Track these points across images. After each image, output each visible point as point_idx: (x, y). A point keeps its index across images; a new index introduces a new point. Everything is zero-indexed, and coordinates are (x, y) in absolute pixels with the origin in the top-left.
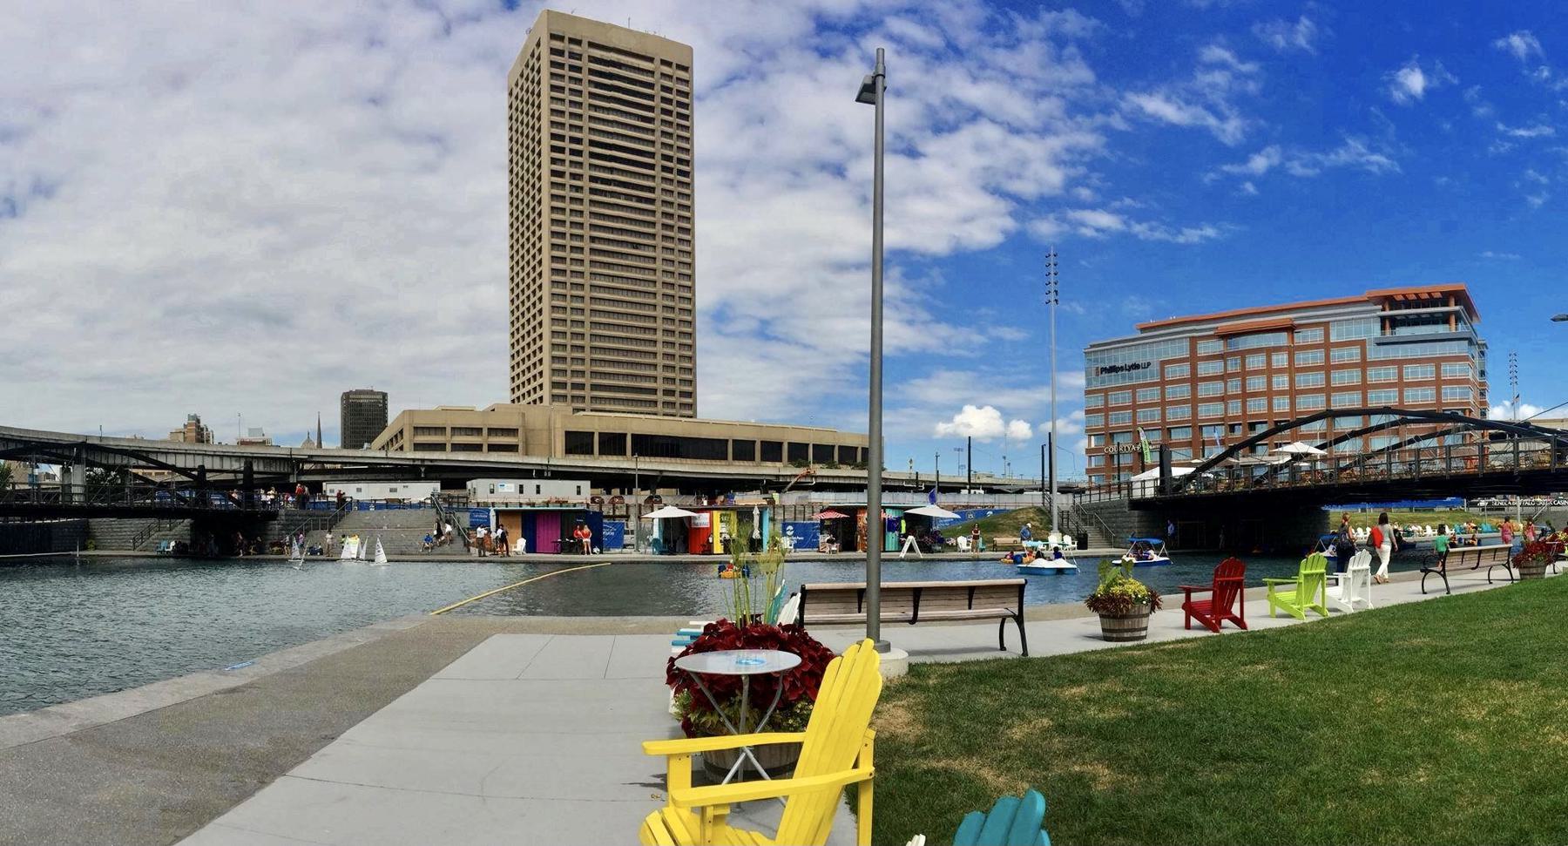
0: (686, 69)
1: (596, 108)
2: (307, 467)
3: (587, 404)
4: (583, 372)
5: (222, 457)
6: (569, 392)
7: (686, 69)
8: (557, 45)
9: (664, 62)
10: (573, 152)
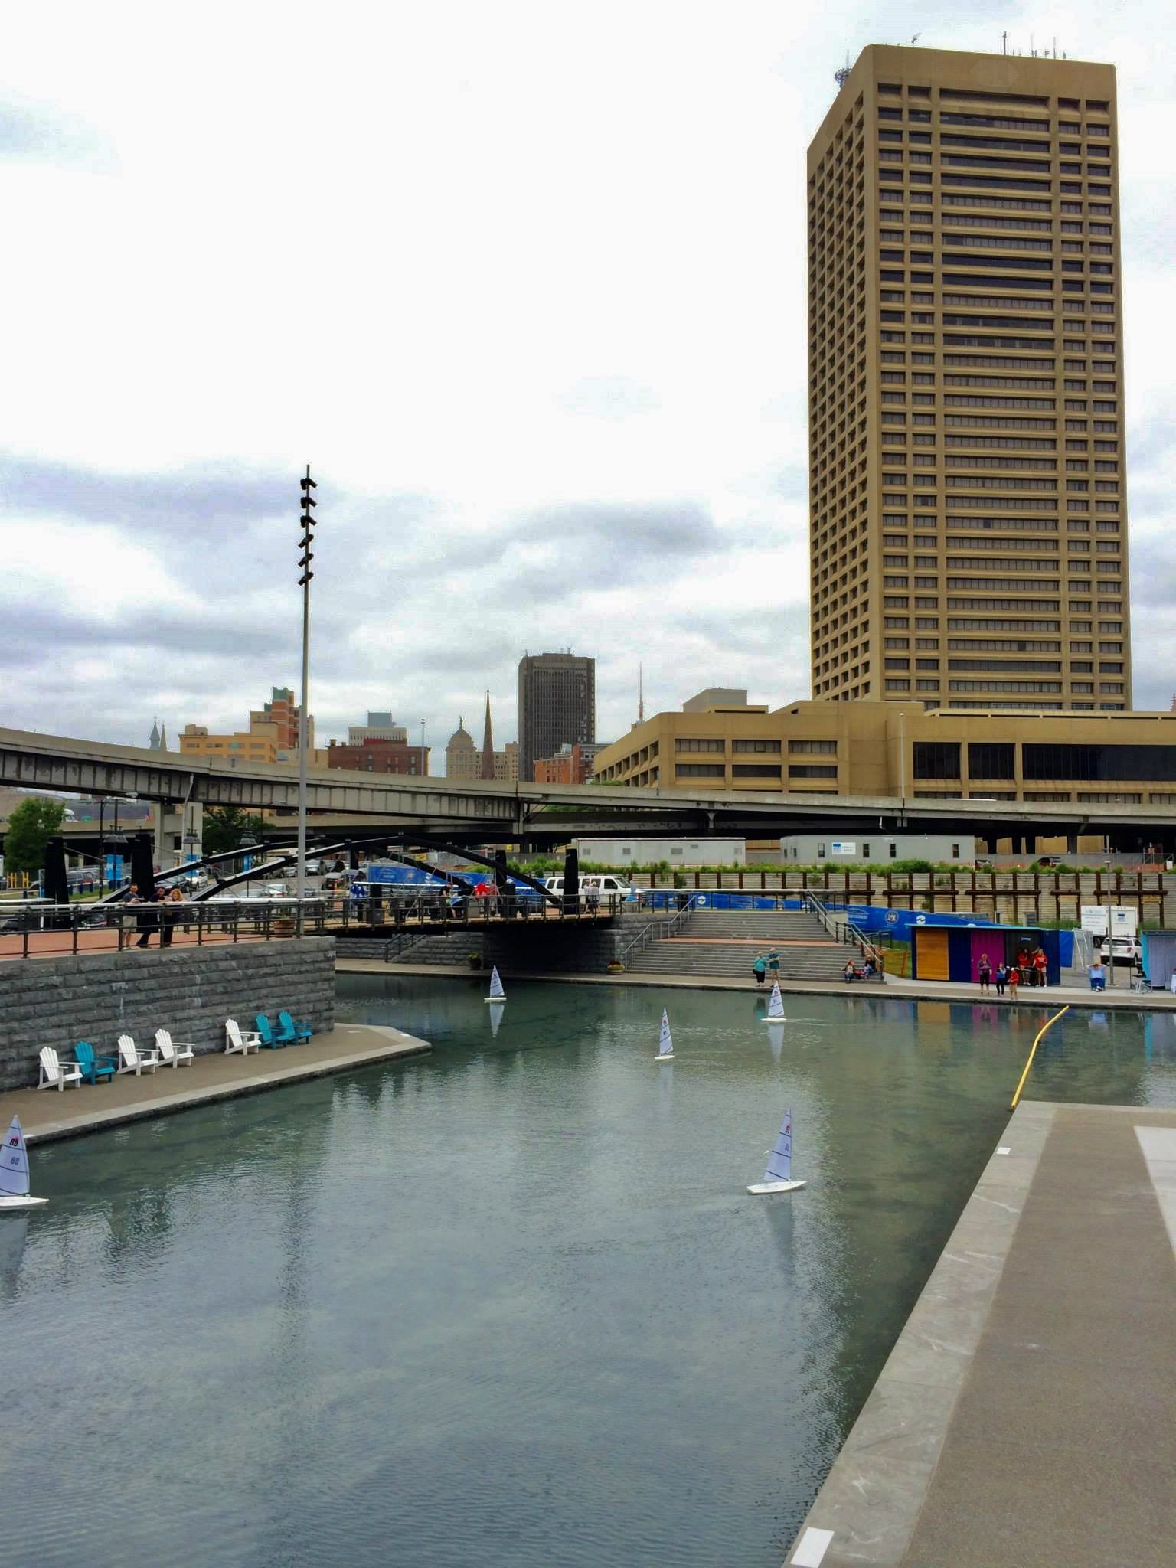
2: (536, 808)
5: (414, 794)
6: (914, 674)
8: (890, 101)
9: (1065, 103)
10: (917, 276)
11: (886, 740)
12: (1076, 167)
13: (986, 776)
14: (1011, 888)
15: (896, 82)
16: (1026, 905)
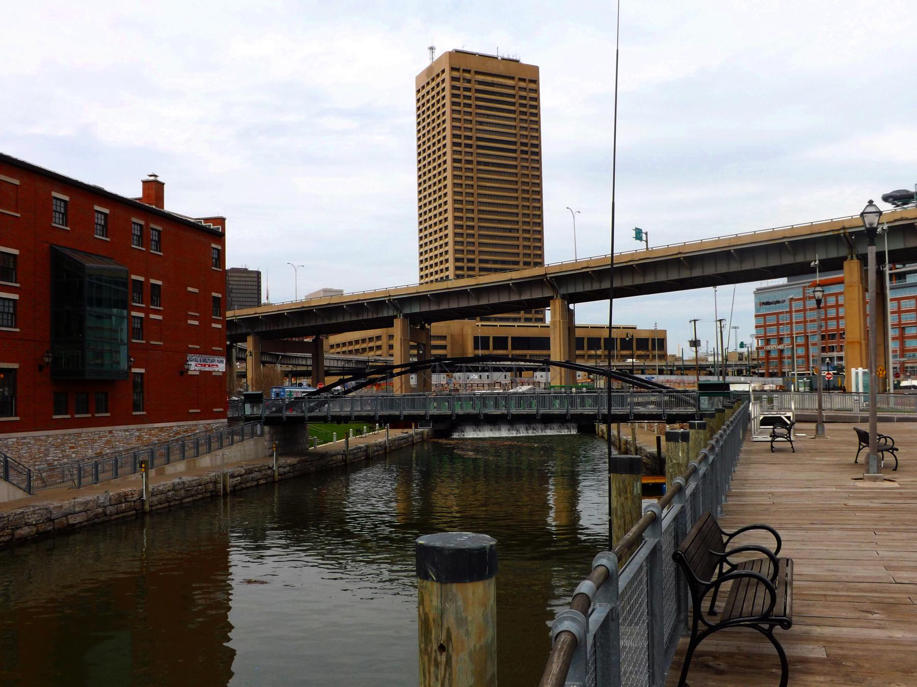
1: (481, 123)
3: (477, 272)
4: (473, 219)
7: (532, 81)
8: (455, 74)
11: (463, 336)
12: (465, 97)
14: (614, 426)
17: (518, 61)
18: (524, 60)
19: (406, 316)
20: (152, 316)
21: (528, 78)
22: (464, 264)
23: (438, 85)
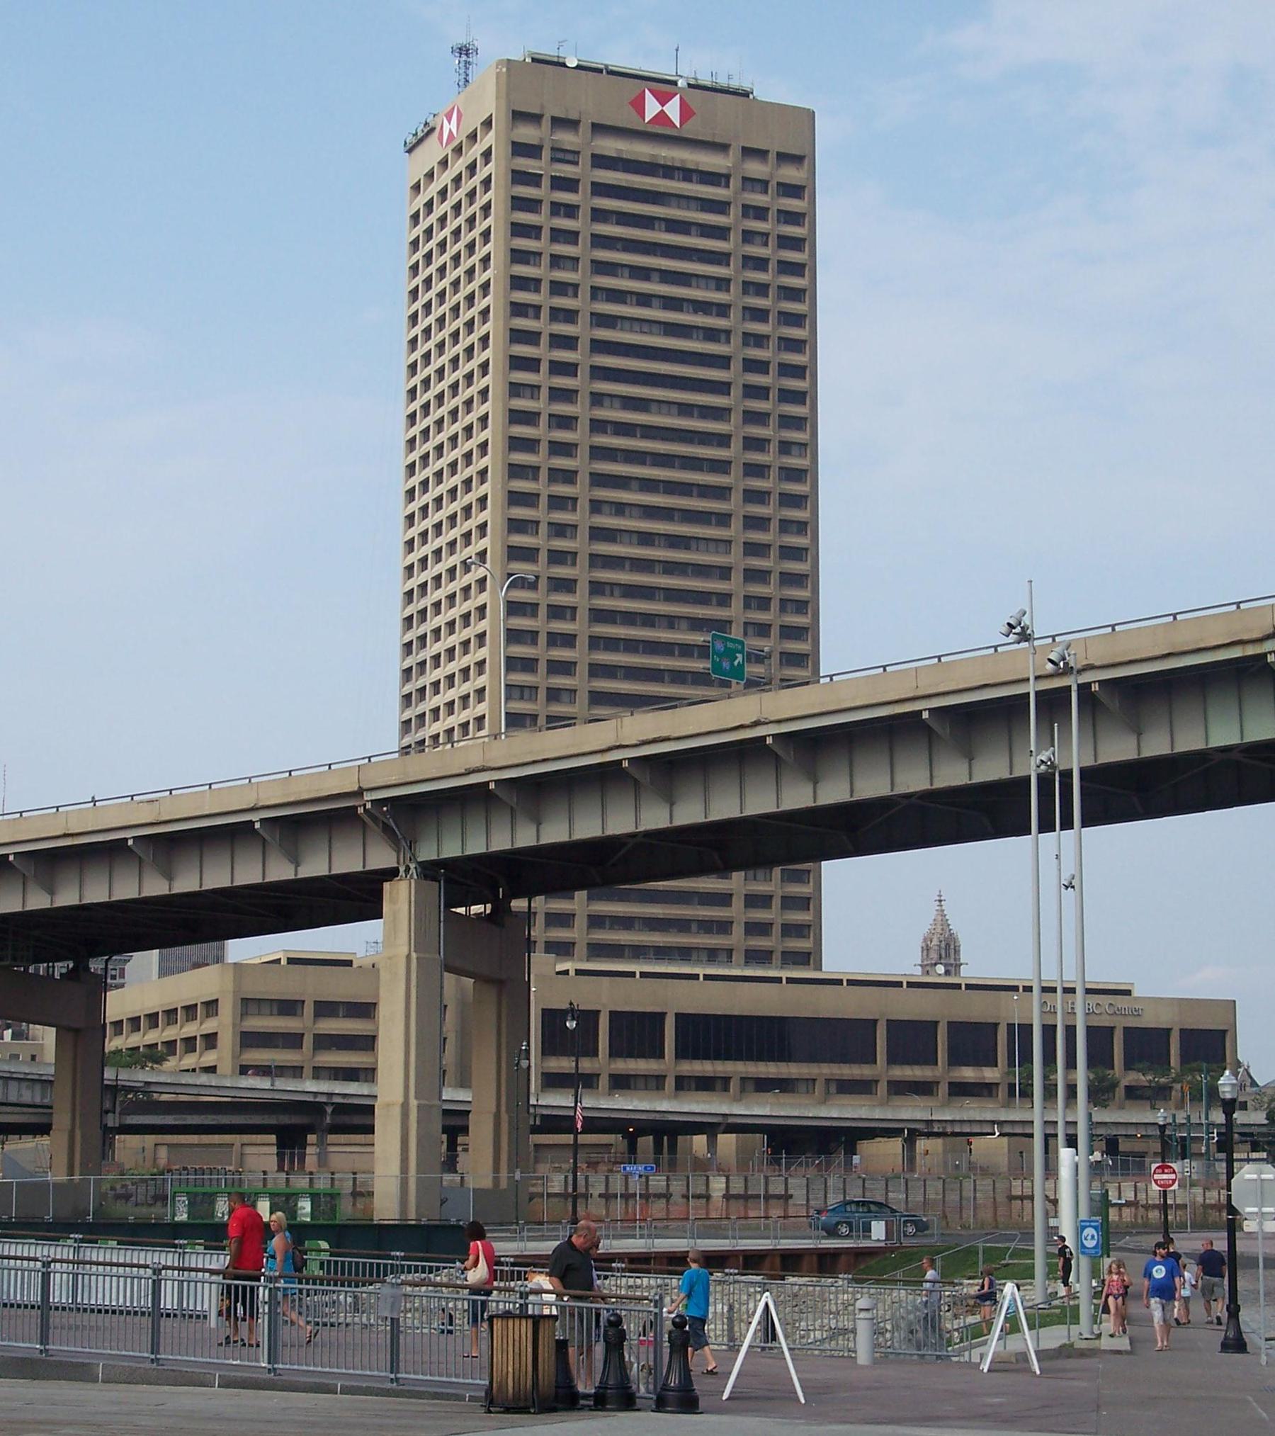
0: (797, 159)
3: (580, 706)
7: (797, 159)
8: (527, 134)
13: (630, 1055)
15: (537, 111)
16: (617, 1186)
17: (746, 94)
18: (769, 91)
19: (429, 871)
20: (1255, 1210)
21: (775, 147)
22: (538, 679)
23: (472, 168)
